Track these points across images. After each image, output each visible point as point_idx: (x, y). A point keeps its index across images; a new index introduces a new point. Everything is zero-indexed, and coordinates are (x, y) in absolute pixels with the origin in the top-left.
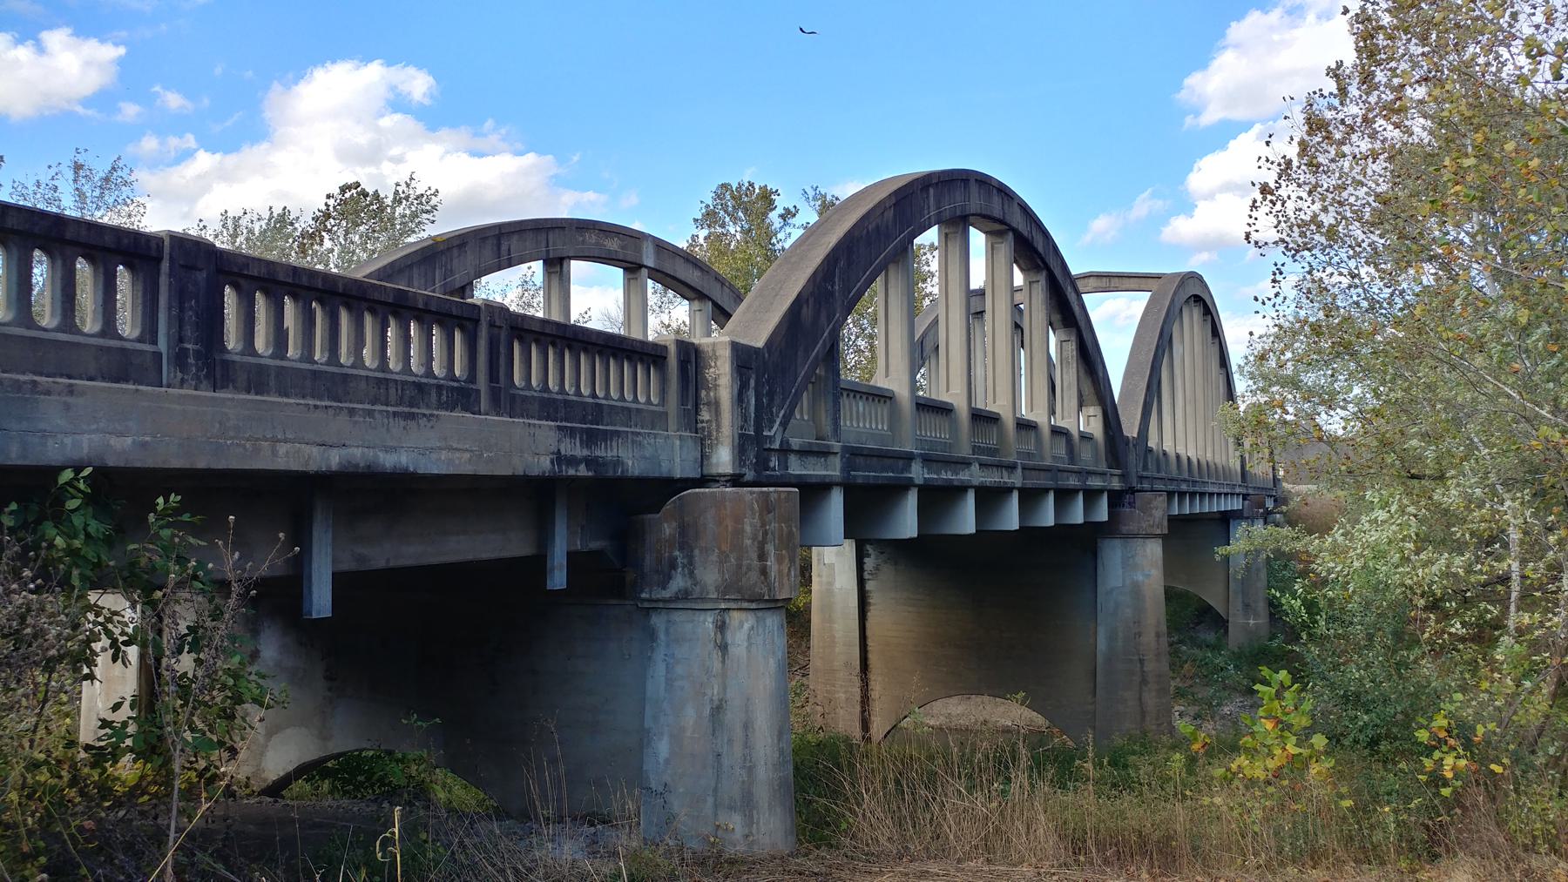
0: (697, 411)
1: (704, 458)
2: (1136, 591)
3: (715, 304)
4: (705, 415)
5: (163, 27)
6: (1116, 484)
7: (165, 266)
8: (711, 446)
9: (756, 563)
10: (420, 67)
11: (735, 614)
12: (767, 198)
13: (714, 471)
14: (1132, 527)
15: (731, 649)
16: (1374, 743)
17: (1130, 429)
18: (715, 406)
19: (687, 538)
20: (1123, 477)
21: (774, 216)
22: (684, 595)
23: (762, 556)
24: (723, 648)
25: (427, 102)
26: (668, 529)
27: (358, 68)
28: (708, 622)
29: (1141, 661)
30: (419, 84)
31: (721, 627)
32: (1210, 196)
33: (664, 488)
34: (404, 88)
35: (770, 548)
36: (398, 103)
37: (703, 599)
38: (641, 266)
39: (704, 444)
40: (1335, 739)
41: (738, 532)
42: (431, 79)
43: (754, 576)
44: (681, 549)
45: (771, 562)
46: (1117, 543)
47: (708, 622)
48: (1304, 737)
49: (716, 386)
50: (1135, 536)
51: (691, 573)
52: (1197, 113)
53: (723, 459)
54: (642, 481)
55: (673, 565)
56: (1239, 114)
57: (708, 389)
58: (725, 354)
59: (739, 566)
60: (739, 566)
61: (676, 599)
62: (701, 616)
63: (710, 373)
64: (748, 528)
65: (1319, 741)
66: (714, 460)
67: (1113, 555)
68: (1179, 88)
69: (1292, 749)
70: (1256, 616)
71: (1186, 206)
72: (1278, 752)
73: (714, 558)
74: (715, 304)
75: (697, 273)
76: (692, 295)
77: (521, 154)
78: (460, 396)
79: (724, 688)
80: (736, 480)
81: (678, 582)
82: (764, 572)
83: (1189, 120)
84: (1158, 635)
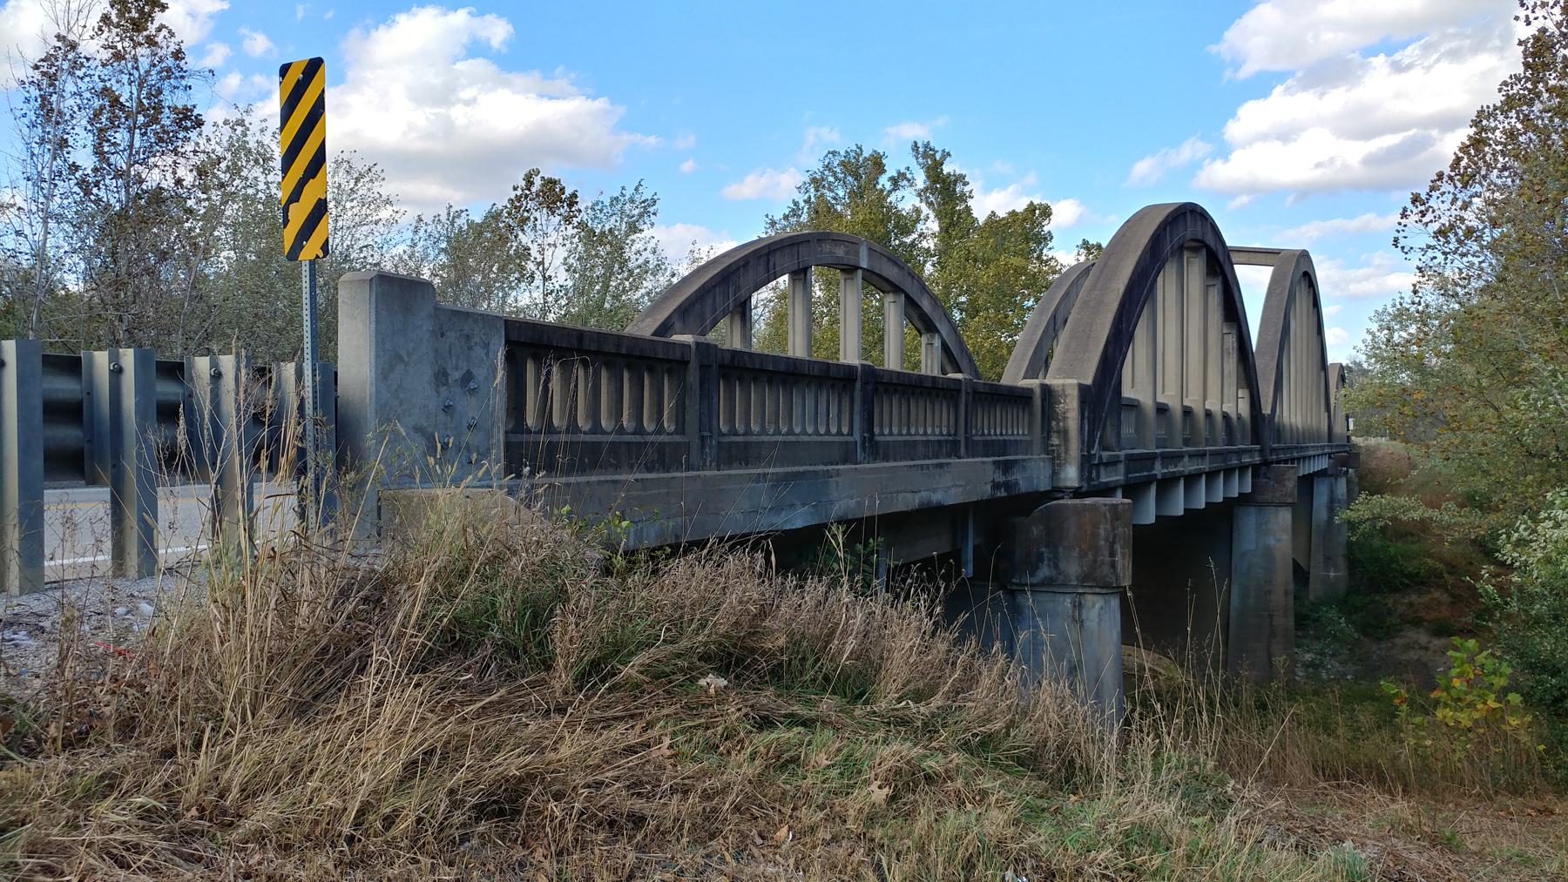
0: (1049, 437)
1: (1055, 474)
2: (1268, 554)
3: (908, 297)
4: (1055, 441)
5: (652, 140)
6: (1257, 459)
7: (858, 385)
8: (1060, 465)
9: (1108, 559)
10: (501, 16)
11: (1089, 597)
12: (878, 164)
13: (1062, 484)
14: (1268, 497)
15: (1087, 624)
16: (1557, 701)
17: (1267, 410)
18: (1064, 434)
19: (1053, 537)
20: (1261, 451)
21: (884, 182)
22: (1049, 582)
23: (1112, 554)
24: (1080, 622)
25: (504, 50)
26: (1036, 531)
27: (445, 14)
28: (1068, 602)
29: (1271, 617)
30: (498, 31)
31: (1079, 606)
32: (1249, 142)
33: (1038, 498)
34: (483, 34)
35: (1118, 547)
36: (476, 49)
37: (1066, 585)
38: (858, 268)
39: (1056, 462)
40: (1527, 697)
41: (1095, 535)
42: (510, 28)
43: (1106, 569)
44: (1047, 546)
45: (1118, 558)
46: (1252, 510)
47: (1068, 602)
48: (1502, 694)
49: (1065, 418)
50: (1269, 504)
51: (1056, 566)
52: (1237, 65)
53: (1071, 475)
54: (1028, 494)
55: (1040, 559)
56: (1281, 66)
57: (1058, 421)
58: (1075, 393)
59: (1095, 561)
60: (1095, 561)
61: (1042, 584)
62: (1061, 598)
63: (1060, 408)
64: (1102, 532)
65: (1514, 698)
66: (1062, 476)
67: (1248, 521)
68: (1217, 37)
69: (1492, 704)
70: (1336, 569)
71: (1223, 151)
72: (1480, 706)
73: (1075, 554)
74: (908, 297)
75: (896, 270)
76: (886, 287)
77: (594, 98)
78: (951, 447)
79: (1079, 653)
80: (1077, 493)
81: (1044, 572)
82: (1113, 565)
83: (1228, 74)
84: (1286, 593)
